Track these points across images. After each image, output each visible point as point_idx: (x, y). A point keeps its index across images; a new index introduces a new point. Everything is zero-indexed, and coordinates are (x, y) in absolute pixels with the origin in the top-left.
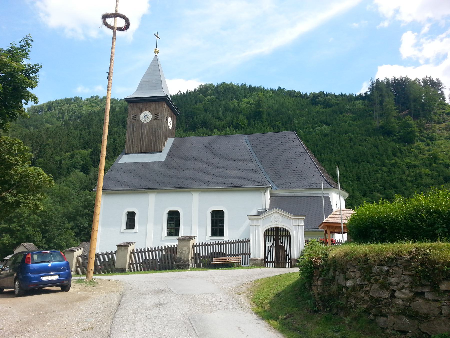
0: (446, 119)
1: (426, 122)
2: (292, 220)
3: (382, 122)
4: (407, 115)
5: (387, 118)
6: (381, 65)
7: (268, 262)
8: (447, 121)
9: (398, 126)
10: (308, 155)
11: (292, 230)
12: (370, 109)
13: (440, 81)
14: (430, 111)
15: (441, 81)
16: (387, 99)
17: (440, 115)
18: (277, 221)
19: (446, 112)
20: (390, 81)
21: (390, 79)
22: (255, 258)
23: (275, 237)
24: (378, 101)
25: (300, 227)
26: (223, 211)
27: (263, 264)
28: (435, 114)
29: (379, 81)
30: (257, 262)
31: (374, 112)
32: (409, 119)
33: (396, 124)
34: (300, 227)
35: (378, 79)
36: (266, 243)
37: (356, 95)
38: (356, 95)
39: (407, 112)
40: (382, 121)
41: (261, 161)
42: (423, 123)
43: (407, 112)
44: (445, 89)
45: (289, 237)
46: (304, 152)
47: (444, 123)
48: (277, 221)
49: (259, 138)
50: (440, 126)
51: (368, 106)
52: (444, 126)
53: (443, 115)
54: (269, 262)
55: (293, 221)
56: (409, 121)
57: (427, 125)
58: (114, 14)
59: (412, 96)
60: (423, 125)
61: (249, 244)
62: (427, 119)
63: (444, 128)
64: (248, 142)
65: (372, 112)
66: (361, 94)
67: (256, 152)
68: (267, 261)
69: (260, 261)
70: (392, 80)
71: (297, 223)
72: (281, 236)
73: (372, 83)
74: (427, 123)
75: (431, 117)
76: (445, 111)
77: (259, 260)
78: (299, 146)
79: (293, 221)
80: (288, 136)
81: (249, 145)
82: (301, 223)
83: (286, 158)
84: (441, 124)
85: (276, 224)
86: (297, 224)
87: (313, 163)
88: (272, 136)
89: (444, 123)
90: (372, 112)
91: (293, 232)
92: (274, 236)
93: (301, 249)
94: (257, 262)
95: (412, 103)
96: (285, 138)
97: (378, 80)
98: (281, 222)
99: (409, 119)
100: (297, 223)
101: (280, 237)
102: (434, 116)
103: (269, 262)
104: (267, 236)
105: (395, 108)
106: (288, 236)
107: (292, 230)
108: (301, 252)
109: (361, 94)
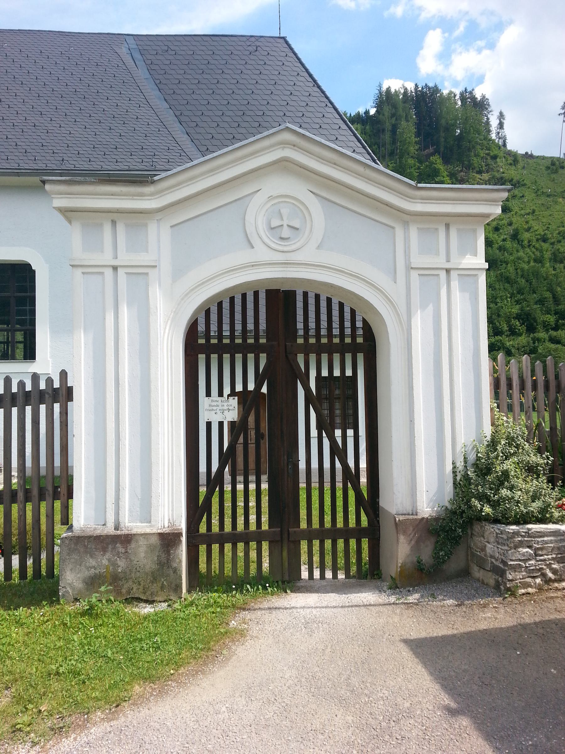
0: (491, 167)
1: (460, 169)
2: (399, 232)
3: (392, 165)
4: (433, 154)
5: (401, 158)
6: (387, 79)
7: (209, 539)
8: (492, 169)
9: (417, 174)
10: (329, 105)
11: (403, 309)
12: (373, 140)
13: (487, 99)
14: (469, 150)
15: (488, 99)
16: (403, 123)
17: (482, 158)
18: (286, 232)
19: (492, 154)
20: (409, 92)
21: (409, 89)
22: (110, 530)
23: (263, 358)
24: (388, 126)
25: (455, 284)
26: (29, 266)
27: (177, 571)
28: (476, 155)
29: (390, 90)
30: (122, 564)
31: (379, 148)
32: (436, 161)
33: (415, 169)
34: (455, 284)
35: (389, 87)
36: (204, 401)
37: (350, 114)
38: (350, 114)
39: (431, 150)
40: (391, 163)
41: (178, 113)
42: (455, 171)
43: (431, 150)
44: (492, 115)
45: (360, 358)
46: (317, 94)
47: (488, 173)
48: (286, 232)
49: (172, 48)
50: (480, 177)
51: (370, 136)
52: (487, 178)
53: (487, 159)
54: (222, 539)
55: (407, 240)
56: (436, 164)
57: (462, 174)
58: (248, 467)
59: (443, 122)
60: (456, 174)
61: (64, 413)
62: (463, 164)
63: (486, 181)
64: (137, 56)
65: (376, 146)
66: (359, 113)
67: (161, 86)
68: (203, 529)
69: (151, 548)
70: (411, 91)
71: (437, 254)
72: (307, 350)
73: (380, 92)
74: (461, 171)
75: (469, 161)
76: (491, 152)
77: (142, 542)
78: (302, 79)
79: (407, 240)
80: (265, 48)
81: (140, 63)
82: (463, 253)
83: (263, 108)
84: (483, 174)
85: (280, 257)
86: (440, 261)
87: (346, 127)
88: (215, 43)
89: (487, 172)
90: (376, 146)
91: (404, 317)
92: (257, 349)
93: (461, 440)
94: (122, 564)
95: (442, 134)
96: (257, 53)
97: (388, 90)
98: (318, 247)
99: (436, 161)
100: (437, 254)
101: (301, 359)
102: (475, 159)
103: (222, 539)
104: (208, 350)
105: (416, 139)
106: (354, 349)
107: (403, 309)
108: (460, 465)
109: (359, 113)
